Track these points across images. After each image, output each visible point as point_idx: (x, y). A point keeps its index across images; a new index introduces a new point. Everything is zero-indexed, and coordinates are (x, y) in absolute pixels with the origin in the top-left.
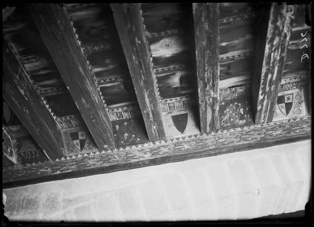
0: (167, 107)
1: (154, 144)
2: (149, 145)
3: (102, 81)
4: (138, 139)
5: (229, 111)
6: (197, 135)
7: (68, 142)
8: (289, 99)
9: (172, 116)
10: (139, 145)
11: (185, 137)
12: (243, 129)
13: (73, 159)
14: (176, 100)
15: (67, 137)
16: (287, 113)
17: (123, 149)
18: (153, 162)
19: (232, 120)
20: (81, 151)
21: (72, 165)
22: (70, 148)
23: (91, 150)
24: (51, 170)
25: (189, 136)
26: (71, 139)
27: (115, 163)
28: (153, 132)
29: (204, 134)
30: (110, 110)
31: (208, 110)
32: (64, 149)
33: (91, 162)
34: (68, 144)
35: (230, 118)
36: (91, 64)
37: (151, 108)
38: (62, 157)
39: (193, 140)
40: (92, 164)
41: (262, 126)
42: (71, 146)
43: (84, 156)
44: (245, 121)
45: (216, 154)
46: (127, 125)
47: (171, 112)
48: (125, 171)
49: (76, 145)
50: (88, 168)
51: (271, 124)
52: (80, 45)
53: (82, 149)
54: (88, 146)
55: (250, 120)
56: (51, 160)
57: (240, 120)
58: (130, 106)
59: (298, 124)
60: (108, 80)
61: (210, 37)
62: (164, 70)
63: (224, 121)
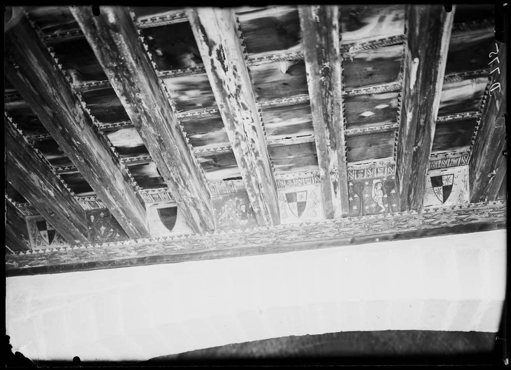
0: (150, 198)
1: (137, 242)
2: (130, 243)
3: (60, 169)
4: (118, 235)
5: (228, 208)
6: (189, 235)
7: (34, 232)
8: (302, 197)
9: (158, 209)
10: (119, 242)
11: (174, 237)
12: (244, 231)
13: (40, 254)
14: (160, 191)
15: (33, 226)
16: (299, 215)
17: (99, 246)
18: (142, 261)
19: (231, 218)
20: (50, 244)
21: (42, 260)
22: (37, 240)
23: (62, 244)
24: (18, 264)
25: (178, 235)
26: (37, 228)
27: (94, 260)
28: (131, 229)
29: (197, 234)
30: (80, 198)
31: (190, 209)
32: (29, 242)
33: (64, 258)
34: (34, 234)
35: (229, 217)
36: (41, 152)
37: (119, 205)
38: (27, 250)
39: (184, 240)
40: (65, 259)
41: (268, 228)
42: (37, 237)
43: (53, 251)
44: (247, 221)
45: (218, 257)
46: (105, 217)
47: (157, 204)
48: (109, 269)
49: (43, 237)
50: (62, 264)
51: (280, 227)
52: (22, 134)
53: (50, 242)
54: (58, 239)
55: (253, 221)
56: (14, 253)
57: (242, 219)
58: (157, 163)
59: (314, 229)
60: (67, 168)
61: (162, 141)
62: (133, 160)
63: (222, 219)
